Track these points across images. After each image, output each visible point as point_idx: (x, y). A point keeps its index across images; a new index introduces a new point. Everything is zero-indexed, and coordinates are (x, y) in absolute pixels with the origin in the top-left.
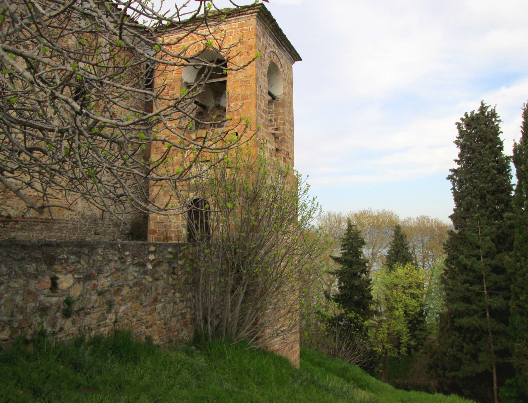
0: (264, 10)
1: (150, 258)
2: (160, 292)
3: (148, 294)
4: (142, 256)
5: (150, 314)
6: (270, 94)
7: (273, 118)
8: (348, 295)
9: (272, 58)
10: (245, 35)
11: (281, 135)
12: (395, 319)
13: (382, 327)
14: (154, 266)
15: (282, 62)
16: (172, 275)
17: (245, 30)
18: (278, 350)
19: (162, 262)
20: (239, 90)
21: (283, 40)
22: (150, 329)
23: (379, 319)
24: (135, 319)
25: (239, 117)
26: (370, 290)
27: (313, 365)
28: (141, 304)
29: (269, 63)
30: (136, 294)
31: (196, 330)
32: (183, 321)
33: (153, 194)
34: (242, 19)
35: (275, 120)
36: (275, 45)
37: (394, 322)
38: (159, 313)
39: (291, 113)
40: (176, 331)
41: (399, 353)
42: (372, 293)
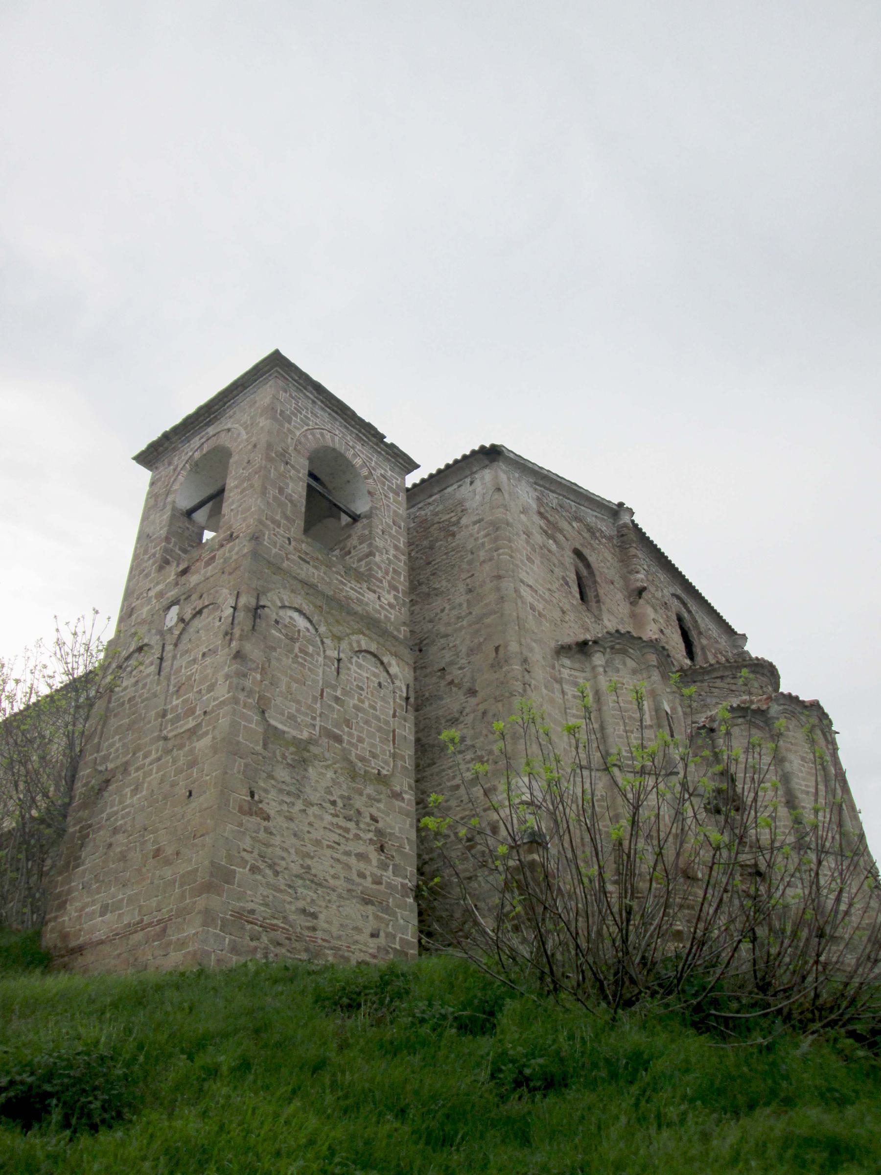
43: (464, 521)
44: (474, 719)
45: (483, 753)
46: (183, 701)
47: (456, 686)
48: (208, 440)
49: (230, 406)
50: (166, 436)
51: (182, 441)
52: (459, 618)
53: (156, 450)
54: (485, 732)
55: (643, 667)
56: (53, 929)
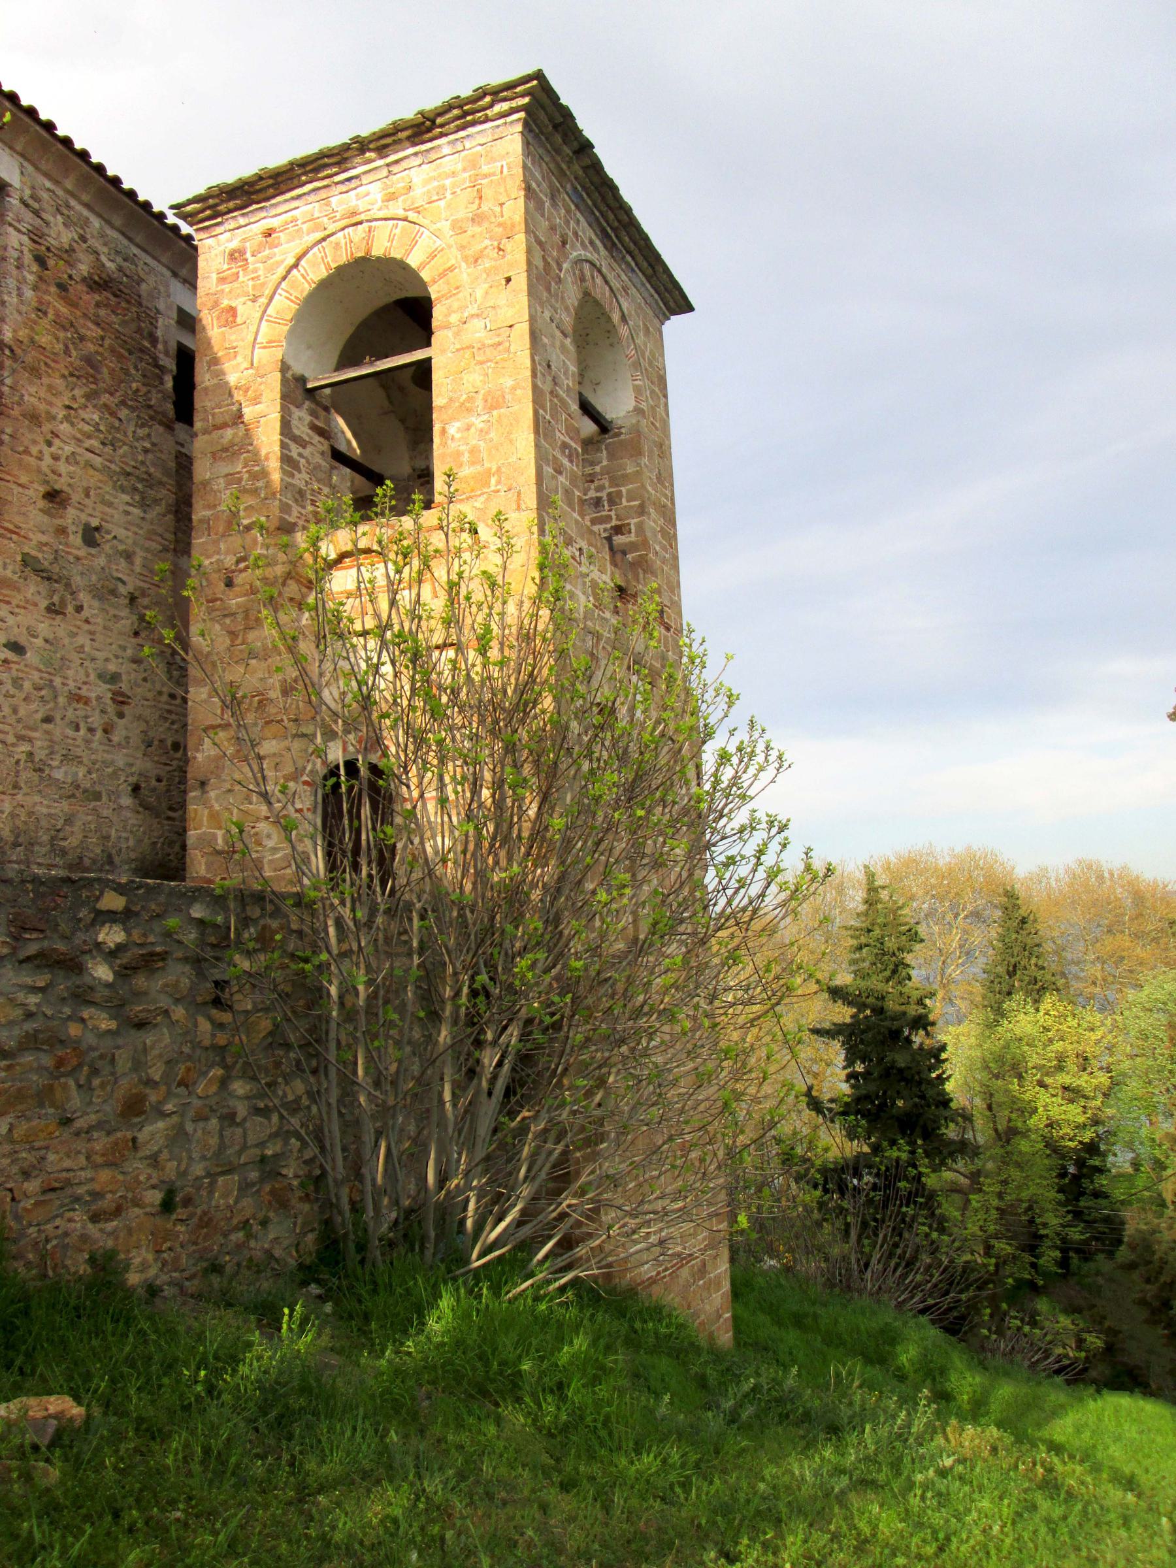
0: (546, 101)
1: (101, 938)
2: (156, 1073)
3: (96, 1082)
4: (63, 927)
5: (109, 1164)
6: (587, 408)
7: (604, 495)
8: (877, 1097)
9: (589, 283)
10: (488, 193)
11: (633, 547)
12: (1018, 1165)
13: (980, 1190)
14: (125, 973)
15: (625, 305)
16: (214, 1012)
17: (485, 176)
18: (653, 1281)
19: (163, 956)
20: (473, 379)
21: (625, 227)
22: (110, 1226)
23: (972, 1168)
24: (32, 1186)
25: (479, 468)
26: (941, 1080)
27: (779, 1323)
28: (66, 1122)
29: (580, 296)
30: (37, 1080)
31: (327, 1222)
32: (268, 1188)
33: (199, 756)
34: (479, 135)
35: (613, 500)
36: (598, 242)
37: (1015, 1174)
38: (154, 1160)
39: (665, 478)
40: (237, 1229)
41: (1034, 1265)
42: (949, 1087)
50: (585, 147)
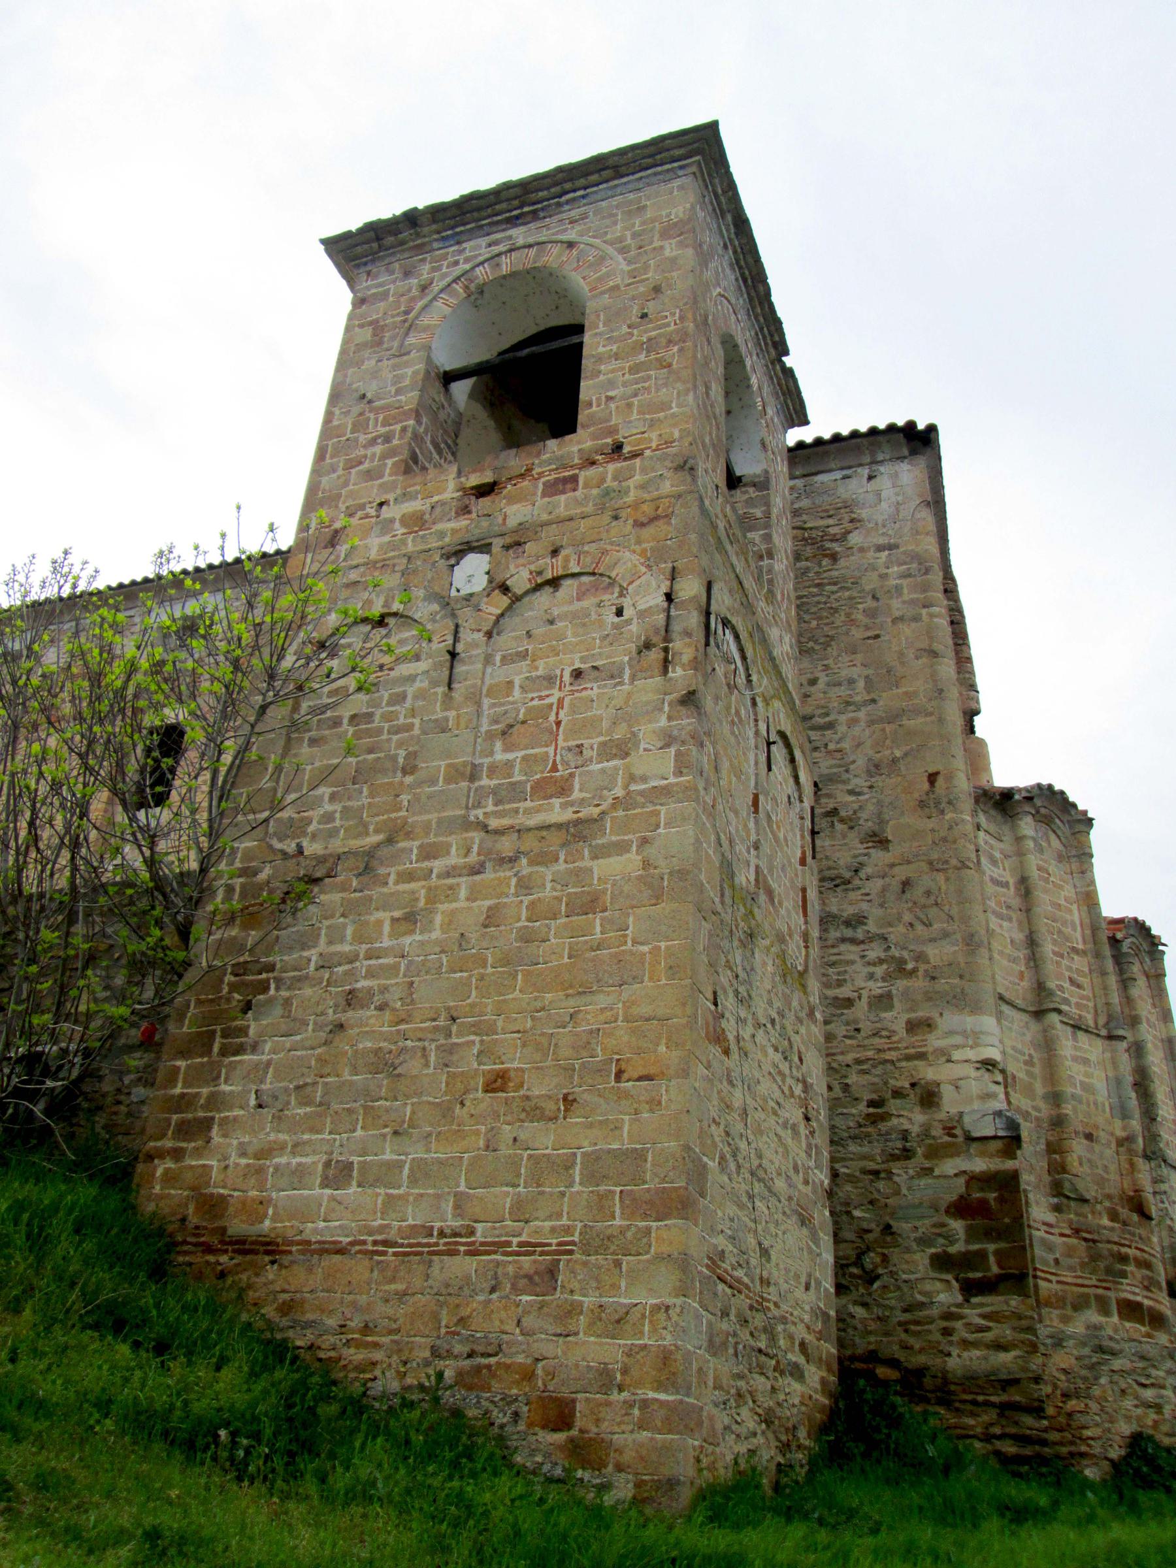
43: (855, 539)
44: (884, 889)
45: (905, 954)
46: (524, 758)
47: (842, 821)
48: (511, 250)
49: (574, 200)
50: (411, 218)
51: (444, 239)
52: (848, 703)
53: (378, 239)
54: (907, 917)
55: (1074, 852)
56: (170, 1179)
